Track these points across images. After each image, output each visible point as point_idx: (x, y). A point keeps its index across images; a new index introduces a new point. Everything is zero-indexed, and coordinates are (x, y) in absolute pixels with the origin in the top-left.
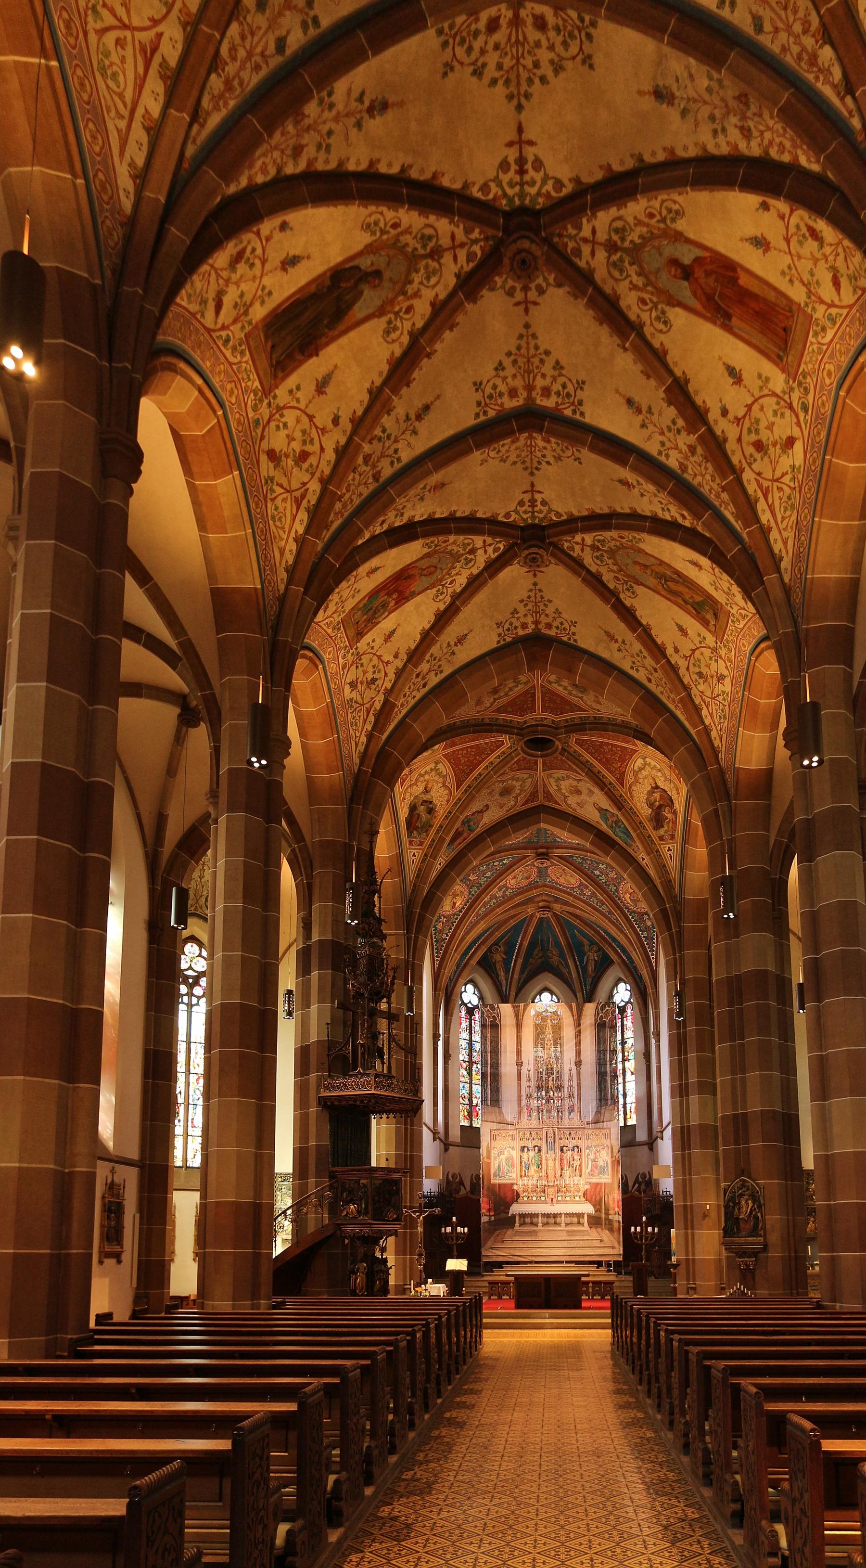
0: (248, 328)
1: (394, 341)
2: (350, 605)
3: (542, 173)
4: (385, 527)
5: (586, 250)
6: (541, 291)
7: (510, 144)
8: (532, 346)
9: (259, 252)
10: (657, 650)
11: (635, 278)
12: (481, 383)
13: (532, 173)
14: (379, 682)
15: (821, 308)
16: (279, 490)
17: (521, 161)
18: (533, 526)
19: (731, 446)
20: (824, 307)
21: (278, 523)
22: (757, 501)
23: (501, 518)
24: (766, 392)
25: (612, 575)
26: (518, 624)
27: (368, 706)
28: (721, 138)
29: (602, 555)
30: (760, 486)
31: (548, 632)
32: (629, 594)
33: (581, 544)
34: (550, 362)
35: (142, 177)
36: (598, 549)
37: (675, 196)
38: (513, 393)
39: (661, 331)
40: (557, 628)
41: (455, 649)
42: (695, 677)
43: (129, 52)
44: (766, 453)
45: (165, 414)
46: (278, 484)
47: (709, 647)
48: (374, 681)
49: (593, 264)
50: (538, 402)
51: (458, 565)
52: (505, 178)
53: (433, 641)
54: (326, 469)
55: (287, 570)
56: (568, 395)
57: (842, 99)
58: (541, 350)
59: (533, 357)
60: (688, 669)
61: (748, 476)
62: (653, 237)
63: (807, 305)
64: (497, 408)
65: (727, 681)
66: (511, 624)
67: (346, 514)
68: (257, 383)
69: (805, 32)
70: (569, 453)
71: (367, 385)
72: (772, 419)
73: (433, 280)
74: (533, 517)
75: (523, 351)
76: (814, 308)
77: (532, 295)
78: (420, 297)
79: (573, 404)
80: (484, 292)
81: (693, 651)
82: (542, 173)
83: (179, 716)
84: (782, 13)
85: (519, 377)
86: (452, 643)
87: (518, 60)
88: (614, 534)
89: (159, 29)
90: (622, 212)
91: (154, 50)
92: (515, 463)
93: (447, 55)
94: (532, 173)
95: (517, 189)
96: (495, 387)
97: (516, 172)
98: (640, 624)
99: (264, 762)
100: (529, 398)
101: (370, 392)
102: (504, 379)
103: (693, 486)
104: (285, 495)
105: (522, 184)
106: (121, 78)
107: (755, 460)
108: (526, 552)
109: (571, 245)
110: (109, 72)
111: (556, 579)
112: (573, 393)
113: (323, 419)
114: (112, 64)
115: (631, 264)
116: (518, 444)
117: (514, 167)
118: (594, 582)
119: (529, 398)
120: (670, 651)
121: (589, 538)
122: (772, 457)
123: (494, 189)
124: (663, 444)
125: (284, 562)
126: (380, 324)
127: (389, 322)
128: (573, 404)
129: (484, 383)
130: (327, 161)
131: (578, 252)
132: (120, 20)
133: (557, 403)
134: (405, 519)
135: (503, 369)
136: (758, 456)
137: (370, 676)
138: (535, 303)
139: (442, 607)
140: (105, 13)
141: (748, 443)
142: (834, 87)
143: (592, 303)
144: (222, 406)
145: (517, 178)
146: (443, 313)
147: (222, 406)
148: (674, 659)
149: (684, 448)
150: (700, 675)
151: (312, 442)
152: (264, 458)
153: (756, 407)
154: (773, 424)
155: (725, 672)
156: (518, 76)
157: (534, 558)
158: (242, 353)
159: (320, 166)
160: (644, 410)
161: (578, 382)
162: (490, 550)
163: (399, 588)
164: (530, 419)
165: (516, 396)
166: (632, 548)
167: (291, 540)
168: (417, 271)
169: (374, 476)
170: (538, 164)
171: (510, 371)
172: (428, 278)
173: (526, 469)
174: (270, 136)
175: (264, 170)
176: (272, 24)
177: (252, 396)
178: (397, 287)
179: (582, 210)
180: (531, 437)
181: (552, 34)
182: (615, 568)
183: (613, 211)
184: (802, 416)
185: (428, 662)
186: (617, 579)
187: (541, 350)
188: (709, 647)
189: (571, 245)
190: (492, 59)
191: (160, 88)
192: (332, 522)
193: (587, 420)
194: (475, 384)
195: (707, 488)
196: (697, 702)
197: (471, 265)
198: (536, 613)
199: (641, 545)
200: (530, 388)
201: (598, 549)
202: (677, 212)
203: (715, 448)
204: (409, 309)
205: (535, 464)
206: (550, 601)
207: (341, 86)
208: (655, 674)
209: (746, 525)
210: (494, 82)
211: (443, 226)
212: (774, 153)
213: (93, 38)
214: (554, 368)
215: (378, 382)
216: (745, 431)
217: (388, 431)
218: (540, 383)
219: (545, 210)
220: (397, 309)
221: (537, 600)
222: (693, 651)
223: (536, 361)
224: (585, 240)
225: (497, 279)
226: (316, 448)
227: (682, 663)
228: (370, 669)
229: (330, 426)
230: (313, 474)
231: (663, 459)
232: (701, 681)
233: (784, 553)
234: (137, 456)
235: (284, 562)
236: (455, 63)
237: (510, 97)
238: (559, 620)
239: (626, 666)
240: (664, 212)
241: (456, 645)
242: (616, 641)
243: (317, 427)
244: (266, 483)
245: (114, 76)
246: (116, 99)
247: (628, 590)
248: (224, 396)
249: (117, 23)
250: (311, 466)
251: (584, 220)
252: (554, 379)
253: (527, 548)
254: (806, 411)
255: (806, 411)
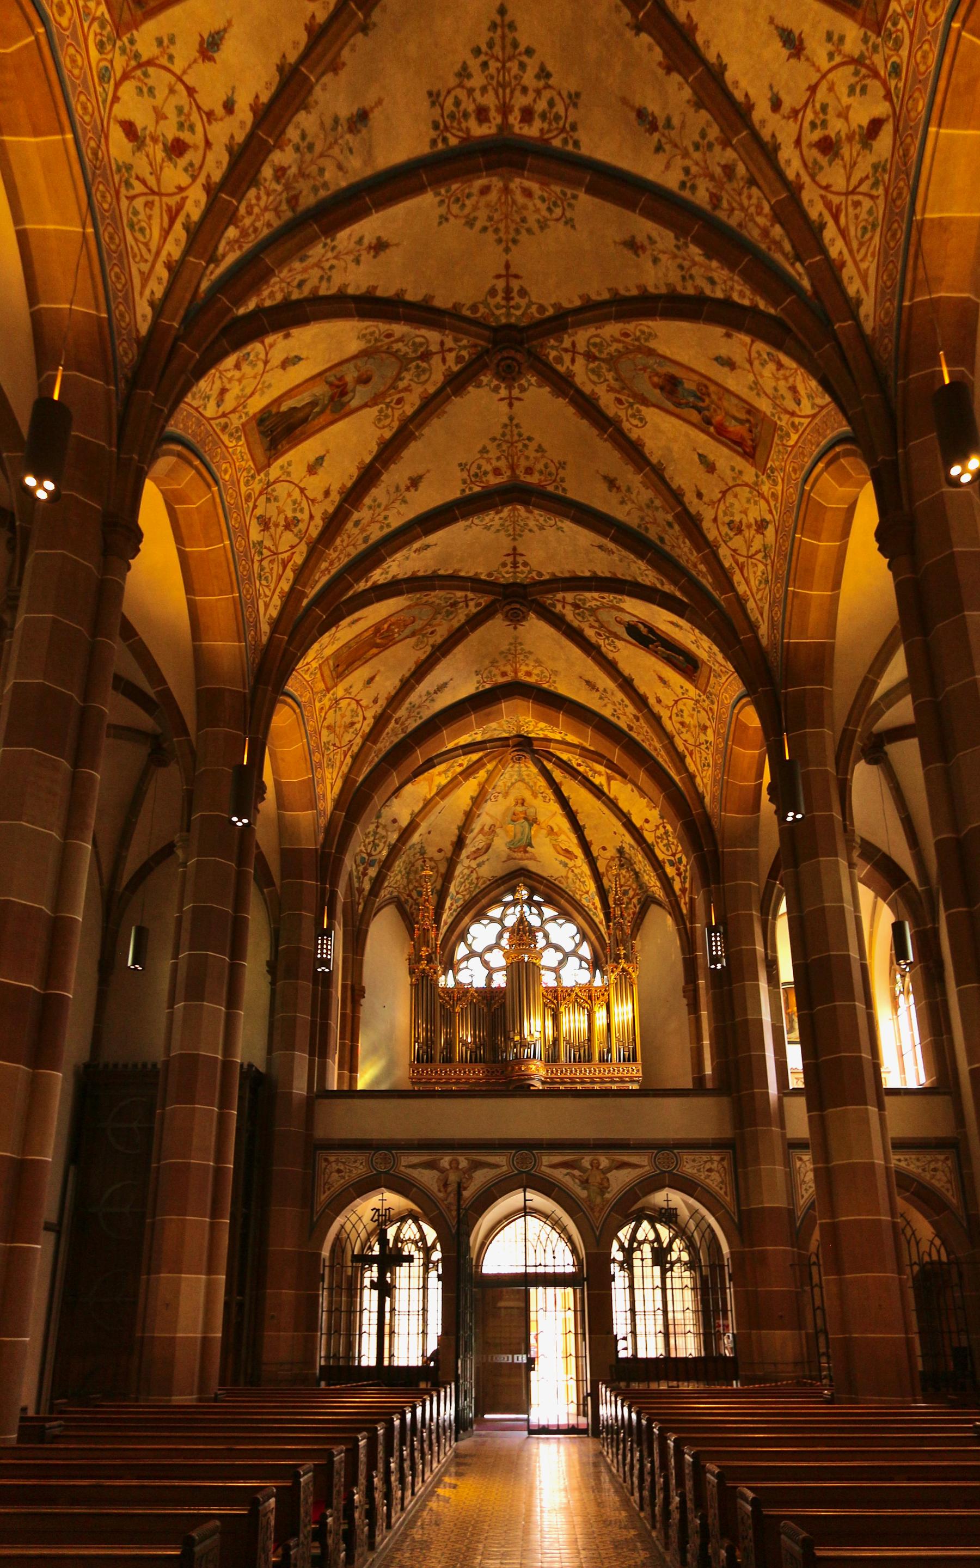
0: (244, 419)
1: (384, 427)
2: (329, 651)
3: (526, 300)
4: (369, 584)
5: (567, 358)
6: (523, 389)
7: (498, 277)
8: (508, 41)
9: (262, 356)
10: (640, 701)
11: (612, 382)
12: (438, 95)
13: (517, 299)
14: (358, 726)
15: (785, 417)
16: (138, 188)
17: (508, 291)
18: (509, 326)
19: (707, 524)
20: (787, 416)
21: (264, 582)
22: (823, 226)
23: (483, 577)
24: (739, 482)
25: (612, 396)
26: (471, 108)
27: (285, 556)
28: (689, 284)
29: (599, 367)
30: (828, 205)
31: (528, 679)
32: (635, 422)
33: (564, 602)
34: (533, 446)
35: (158, 308)
36: (595, 358)
37: (650, 323)
38: (497, 472)
39: (636, 426)
40: (541, 472)
41: (407, 494)
42: (678, 726)
43: (156, 211)
44: (837, 155)
45: (161, 491)
46: (138, 178)
47: (747, 485)
48: (352, 724)
49: (564, 611)
50: (522, 478)
51: (439, 617)
52: (492, 302)
53: (413, 688)
54: (314, 532)
55: (151, 304)
56: (557, 117)
57: (793, 265)
58: (522, 48)
59: (510, 59)
60: (670, 718)
61: (723, 552)
62: (628, 351)
63: (773, 415)
64: (460, 134)
65: (710, 731)
66: (479, 467)
67: (246, 247)
68: (251, 463)
69: (759, 214)
70: (552, 522)
71: (276, 59)
72: (845, 100)
73: (423, 378)
74: (508, 315)
75: (508, 437)
76: (780, 419)
77: (516, 392)
78: (411, 391)
79: (563, 130)
80: (470, 389)
81: (676, 702)
82: (526, 300)
83: (150, 755)
84: (737, 198)
85: (491, 93)
86: (403, 487)
87: (504, 67)
88: (596, 595)
89: (184, 194)
90: (599, 331)
91: (178, 212)
92: (498, 531)
93: (443, 210)
94: (517, 299)
95: (504, 310)
96: (479, 467)
97: (504, 298)
98: (647, 462)
99: (245, 821)
100: (514, 475)
101: (280, 69)
102: (488, 460)
103: (730, 228)
104: (150, 198)
105: (508, 308)
106: (148, 231)
107: (821, 168)
108: (508, 608)
109: (553, 354)
110: (137, 228)
111: (536, 631)
112: (562, 113)
113: (315, 491)
114: (139, 221)
115: (609, 370)
116: (501, 515)
117: (501, 294)
118: (587, 406)
119: (514, 475)
120: (652, 701)
121: (570, 597)
122: (847, 157)
123: (482, 310)
124: (687, 171)
125: (147, 292)
126: (373, 412)
127: (381, 411)
128: (563, 130)
129: (443, 94)
130: (328, 289)
131: (559, 360)
132: (151, 190)
133: (542, 130)
134: (389, 577)
135: (487, 452)
136: (823, 161)
137: (348, 720)
138: (519, 399)
139: (388, 434)
140: (136, 183)
141: (811, 146)
142: (786, 255)
143: (573, 402)
144: (216, 482)
145: (503, 303)
146: (431, 406)
147: (216, 482)
148: (657, 708)
149: (718, 171)
150: (682, 724)
151: (302, 510)
152: (117, 134)
153: (824, 86)
154: (848, 107)
155: (708, 724)
156: (503, 48)
157: (509, 366)
158: (239, 439)
159: (322, 292)
160: (661, 124)
161: (570, 96)
162: (471, 604)
163: (381, 638)
164: (504, 154)
165: (487, 120)
166: (639, 349)
167: (276, 597)
168: (407, 370)
169: (289, 201)
170: (523, 293)
171: (477, 81)
172: (418, 376)
173: (499, 241)
174: (280, 272)
175: (272, 295)
176: (305, 270)
177: (96, 26)
178: (390, 382)
179: (564, 329)
180: (514, 509)
181: (538, 203)
182: (596, 625)
183: (592, 331)
184: (772, 503)
185: (370, 508)
186: (620, 401)
187: (522, 48)
188: (747, 485)
189: (553, 354)
190: (482, 214)
191: (183, 235)
192: (224, 256)
193: (585, 151)
194: (430, 94)
195: (685, 558)
196: (727, 565)
197: (459, 366)
198: (503, 85)
199: (622, 605)
200: (505, 110)
201: (595, 358)
202: (650, 334)
203: (691, 525)
204: (399, 401)
205: (512, 234)
206: (530, 653)
207: (343, 235)
208: (671, 531)
209: (679, 773)
210: (485, 229)
211: (433, 336)
212: (736, 297)
213: (124, 203)
214: (538, 77)
215: (407, 675)
216: (806, 125)
217: (309, 139)
218: (523, 463)
219: (529, 327)
220: (388, 400)
221: (510, 437)
222: (676, 702)
223: (520, 445)
224: (566, 350)
225: (482, 378)
226: (306, 516)
227: (665, 714)
228: (348, 713)
229: (219, 111)
230: (194, 178)
231: (686, 194)
232: (684, 730)
233: (863, 295)
234: (137, 536)
235: (147, 292)
236: (449, 216)
237: (499, 241)
238: (543, 461)
239: (607, 712)
240: (638, 334)
241: (408, 489)
242: (618, 489)
243: (199, 108)
244: (119, 170)
245: (142, 230)
246: (141, 246)
247: (633, 416)
248: (299, 699)
249: (146, 190)
250: (191, 164)
251: (566, 336)
252: (538, 92)
253: (509, 604)
254: (776, 500)
255: (776, 500)
